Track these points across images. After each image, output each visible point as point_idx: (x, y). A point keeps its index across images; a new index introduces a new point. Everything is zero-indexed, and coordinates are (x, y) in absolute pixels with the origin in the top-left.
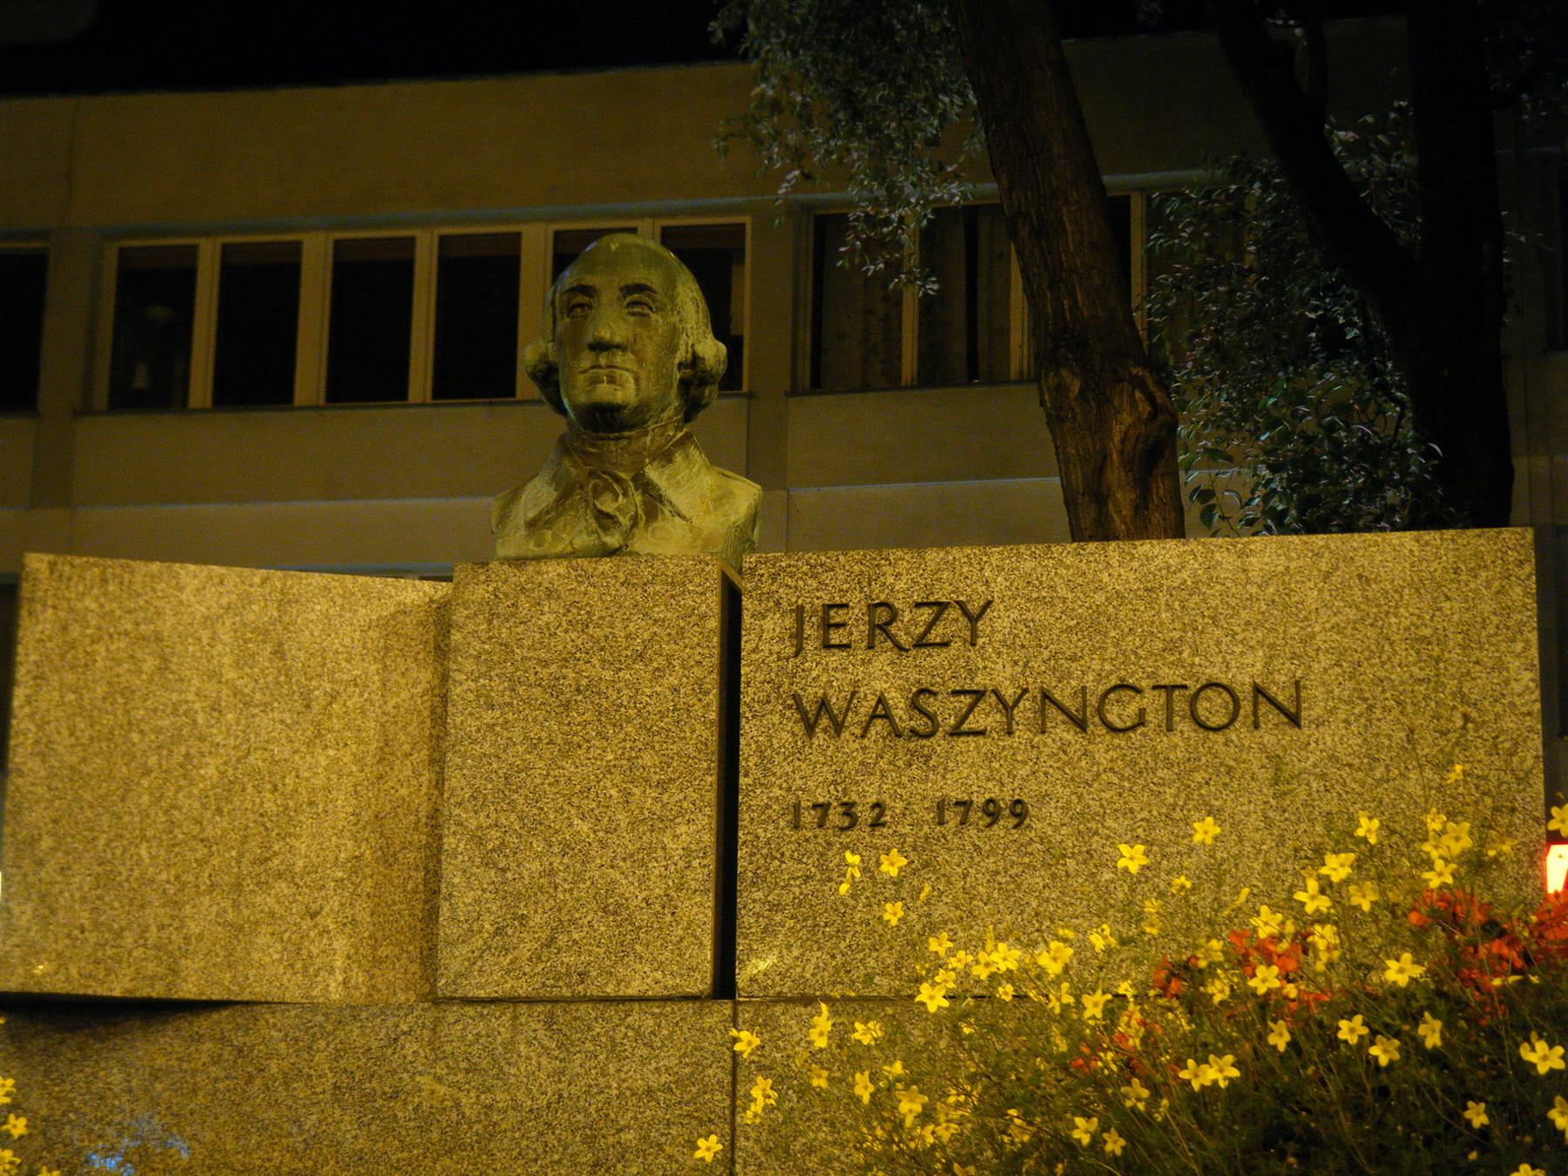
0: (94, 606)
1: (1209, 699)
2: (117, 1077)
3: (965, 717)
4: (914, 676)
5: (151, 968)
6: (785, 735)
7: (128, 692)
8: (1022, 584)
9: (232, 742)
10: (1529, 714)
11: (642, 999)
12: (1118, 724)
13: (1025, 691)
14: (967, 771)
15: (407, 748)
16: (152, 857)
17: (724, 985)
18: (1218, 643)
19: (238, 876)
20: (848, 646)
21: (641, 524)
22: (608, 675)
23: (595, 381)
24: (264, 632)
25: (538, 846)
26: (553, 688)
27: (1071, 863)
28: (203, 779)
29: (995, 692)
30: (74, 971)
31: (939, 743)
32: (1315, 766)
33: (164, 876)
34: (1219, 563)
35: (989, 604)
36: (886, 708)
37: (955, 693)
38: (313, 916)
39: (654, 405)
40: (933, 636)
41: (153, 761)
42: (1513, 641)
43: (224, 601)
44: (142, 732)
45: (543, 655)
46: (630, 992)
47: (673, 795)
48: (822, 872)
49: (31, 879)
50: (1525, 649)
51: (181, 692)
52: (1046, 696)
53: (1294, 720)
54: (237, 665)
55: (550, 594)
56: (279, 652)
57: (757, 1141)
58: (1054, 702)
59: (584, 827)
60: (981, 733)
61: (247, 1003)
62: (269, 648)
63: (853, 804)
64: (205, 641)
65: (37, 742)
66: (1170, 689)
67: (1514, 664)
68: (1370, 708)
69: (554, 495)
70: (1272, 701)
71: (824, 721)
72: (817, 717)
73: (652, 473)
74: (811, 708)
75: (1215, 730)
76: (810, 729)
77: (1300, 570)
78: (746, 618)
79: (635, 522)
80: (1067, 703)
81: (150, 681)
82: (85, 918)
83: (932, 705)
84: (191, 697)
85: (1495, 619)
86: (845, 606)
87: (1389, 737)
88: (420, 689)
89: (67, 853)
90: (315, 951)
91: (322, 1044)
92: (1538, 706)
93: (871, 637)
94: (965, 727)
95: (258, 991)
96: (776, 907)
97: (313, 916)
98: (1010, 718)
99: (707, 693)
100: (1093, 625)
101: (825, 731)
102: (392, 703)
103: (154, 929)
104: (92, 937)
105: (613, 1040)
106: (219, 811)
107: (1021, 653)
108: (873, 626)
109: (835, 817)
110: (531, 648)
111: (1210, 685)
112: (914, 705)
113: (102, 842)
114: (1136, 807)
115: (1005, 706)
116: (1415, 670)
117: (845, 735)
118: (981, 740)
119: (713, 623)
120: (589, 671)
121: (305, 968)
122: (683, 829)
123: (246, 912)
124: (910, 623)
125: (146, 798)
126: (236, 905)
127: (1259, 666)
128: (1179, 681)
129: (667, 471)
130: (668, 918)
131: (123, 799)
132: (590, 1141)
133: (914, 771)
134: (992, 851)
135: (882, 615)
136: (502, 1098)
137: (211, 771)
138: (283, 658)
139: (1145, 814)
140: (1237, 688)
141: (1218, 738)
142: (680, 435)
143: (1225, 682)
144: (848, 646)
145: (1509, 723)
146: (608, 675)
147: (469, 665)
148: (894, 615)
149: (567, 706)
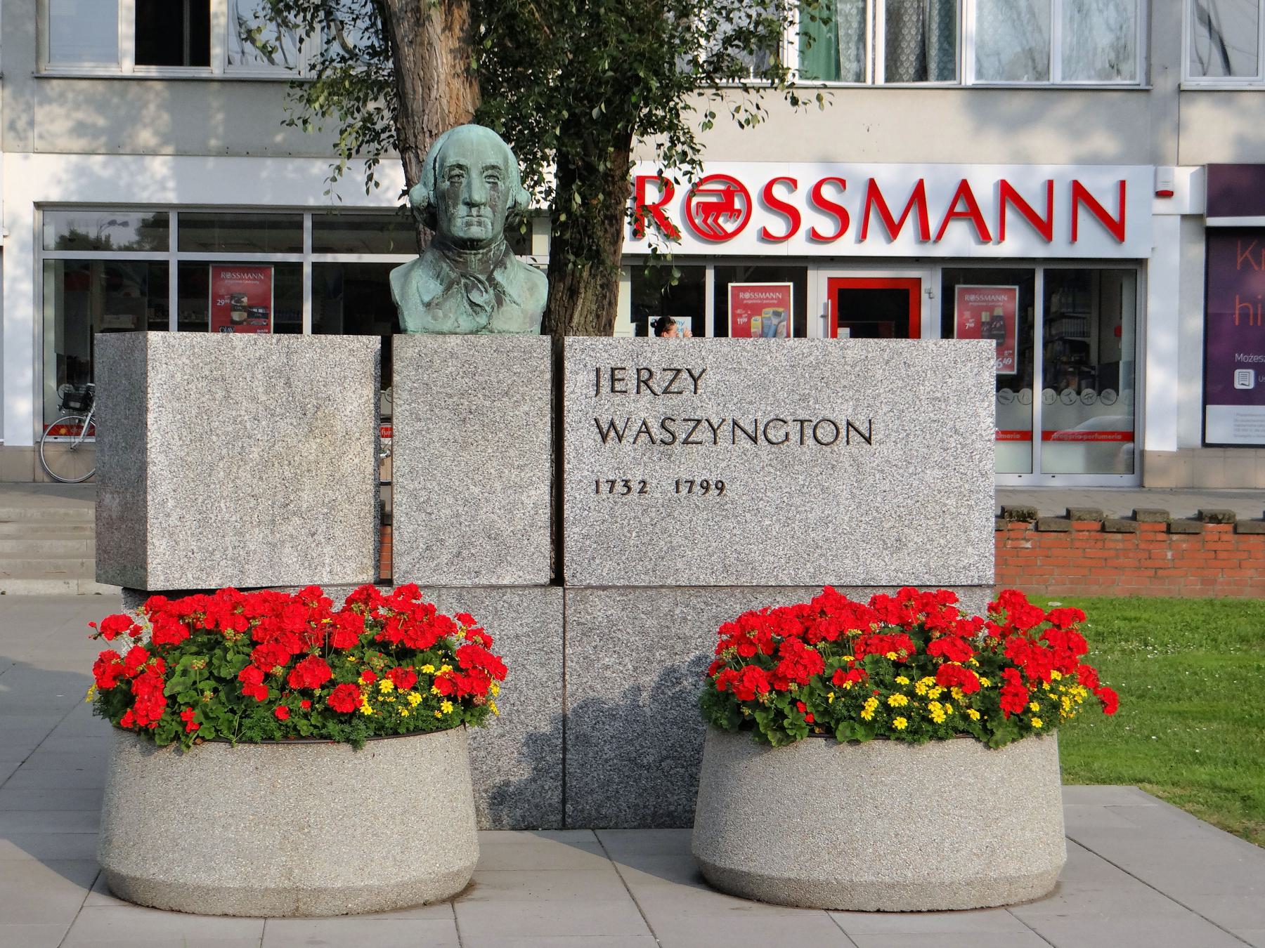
3: (690, 434)
4: (662, 410)
5: (230, 571)
6: (591, 441)
7: (208, 412)
11: (513, 587)
12: (774, 440)
14: (693, 463)
17: (558, 579)
18: (829, 397)
22: (487, 403)
23: (469, 224)
25: (450, 500)
26: (455, 411)
27: (748, 515)
30: (190, 576)
33: (234, 519)
35: (704, 371)
38: (313, 535)
40: (673, 388)
41: (224, 451)
42: (983, 401)
46: (505, 582)
52: (735, 423)
53: (868, 441)
54: (266, 392)
55: (452, 355)
56: (288, 384)
59: (476, 490)
66: (802, 422)
67: (983, 413)
68: (908, 435)
69: (442, 288)
71: (612, 434)
73: (498, 275)
74: (605, 427)
77: (873, 358)
78: (567, 372)
80: (747, 428)
84: (243, 413)
85: (974, 389)
93: (638, 387)
94: (690, 439)
100: (762, 386)
102: (349, 408)
107: (722, 399)
109: (619, 487)
112: (663, 426)
118: (700, 447)
119: (548, 376)
120: (476, 401)
124: (658, 383)
126: (272, 532)
128: (807, 418)
133: (662, 463)
134: (705, 508)
135: (645, 375)
141: (828, 449)
145: (978, 445)
147: (405, 395)
149: (464, 420)
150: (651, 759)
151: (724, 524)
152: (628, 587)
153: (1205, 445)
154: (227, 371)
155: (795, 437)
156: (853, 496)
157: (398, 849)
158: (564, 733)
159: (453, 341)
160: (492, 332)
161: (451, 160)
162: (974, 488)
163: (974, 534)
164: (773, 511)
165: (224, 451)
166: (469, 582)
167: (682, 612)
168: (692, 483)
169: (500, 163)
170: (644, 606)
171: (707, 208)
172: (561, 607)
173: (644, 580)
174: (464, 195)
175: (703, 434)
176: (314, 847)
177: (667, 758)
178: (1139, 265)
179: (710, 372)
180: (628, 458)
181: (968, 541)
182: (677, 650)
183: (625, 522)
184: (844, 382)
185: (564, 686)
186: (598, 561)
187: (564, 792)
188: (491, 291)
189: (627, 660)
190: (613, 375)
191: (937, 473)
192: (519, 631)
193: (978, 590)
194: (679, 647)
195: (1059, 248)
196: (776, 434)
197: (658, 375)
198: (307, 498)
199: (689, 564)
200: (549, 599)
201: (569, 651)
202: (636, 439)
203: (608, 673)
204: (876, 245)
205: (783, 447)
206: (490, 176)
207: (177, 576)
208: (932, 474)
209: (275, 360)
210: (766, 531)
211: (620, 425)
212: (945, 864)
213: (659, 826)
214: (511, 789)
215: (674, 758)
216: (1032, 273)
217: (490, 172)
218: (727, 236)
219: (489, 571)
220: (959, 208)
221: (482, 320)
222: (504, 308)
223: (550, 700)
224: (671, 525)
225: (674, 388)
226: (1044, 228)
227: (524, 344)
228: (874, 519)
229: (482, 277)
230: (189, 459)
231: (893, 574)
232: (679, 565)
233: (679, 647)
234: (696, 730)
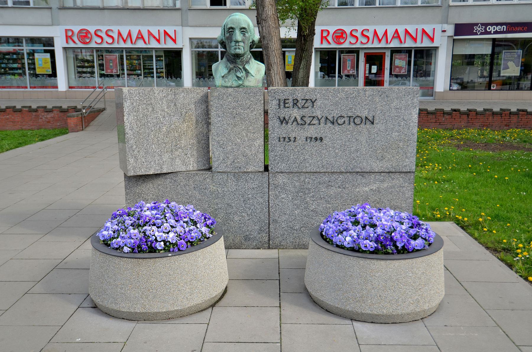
2: (151, 185)
4: (302, 113)
11: (251, 172)
12: (340, 123)
14: (312, 131)
17: (266, 168)
22: (242, 111)
25: (230, 144)
27: (331, 149)
41: (153, 129)
53: (373, 123)
55: (230, 95)
56: (175, 105)
66: (350, 117)
71: (285, 121)
72: (283, 121)
73: (247, 67)
74: (282, 119)
76: (282, 123)
82: (144, 160)
83: (305, 119)
95: (178, 170)
96: (276, 156)
104: (146, 164)
109: (287, 140)
126: (172, 154)
133: (302, 131)
135: (295, 102)
136: (226, 189)
141: (359, 126)
145: (412, 124)
146: (242, 111)
147: (214, 109)
150: (297, 227)
151: (323, 151)
152: (290, 172)
153: (450, 90)
155: (347, 122)
157: (189, 294)
159: (230, 90)
161: (229, 26)
163: (409, 155)
165: (153, 129)
169: (246, 26)
170: (296, 179)
171: (337, 37)
174: (234, 39)
175: (315, 121)
176: (154, 297)
178: (436, 48)
182: (306, 193)
184: (365, 103)
187: (269, 237)
188: (244, 72)
191: (396, 134)
193: (409, 174)
194: (307, 192)
195: (419, 45)
196: (340, 121)
199: (310, 165)
200: (264, 176)
204: (376, 45)
206: (243, 31)
211: (287, 118)
212: (399, 307)
213: (300, 248)
216: (411, 51)
217: (243, 30)
218: (342, 43)
220: (395, 35)
221: (241, 82)
222: (249, 78)
226: (415, 40)
229: (241, 67)
232: (307, 165)
233: (307, 192)
234: (312, 218)
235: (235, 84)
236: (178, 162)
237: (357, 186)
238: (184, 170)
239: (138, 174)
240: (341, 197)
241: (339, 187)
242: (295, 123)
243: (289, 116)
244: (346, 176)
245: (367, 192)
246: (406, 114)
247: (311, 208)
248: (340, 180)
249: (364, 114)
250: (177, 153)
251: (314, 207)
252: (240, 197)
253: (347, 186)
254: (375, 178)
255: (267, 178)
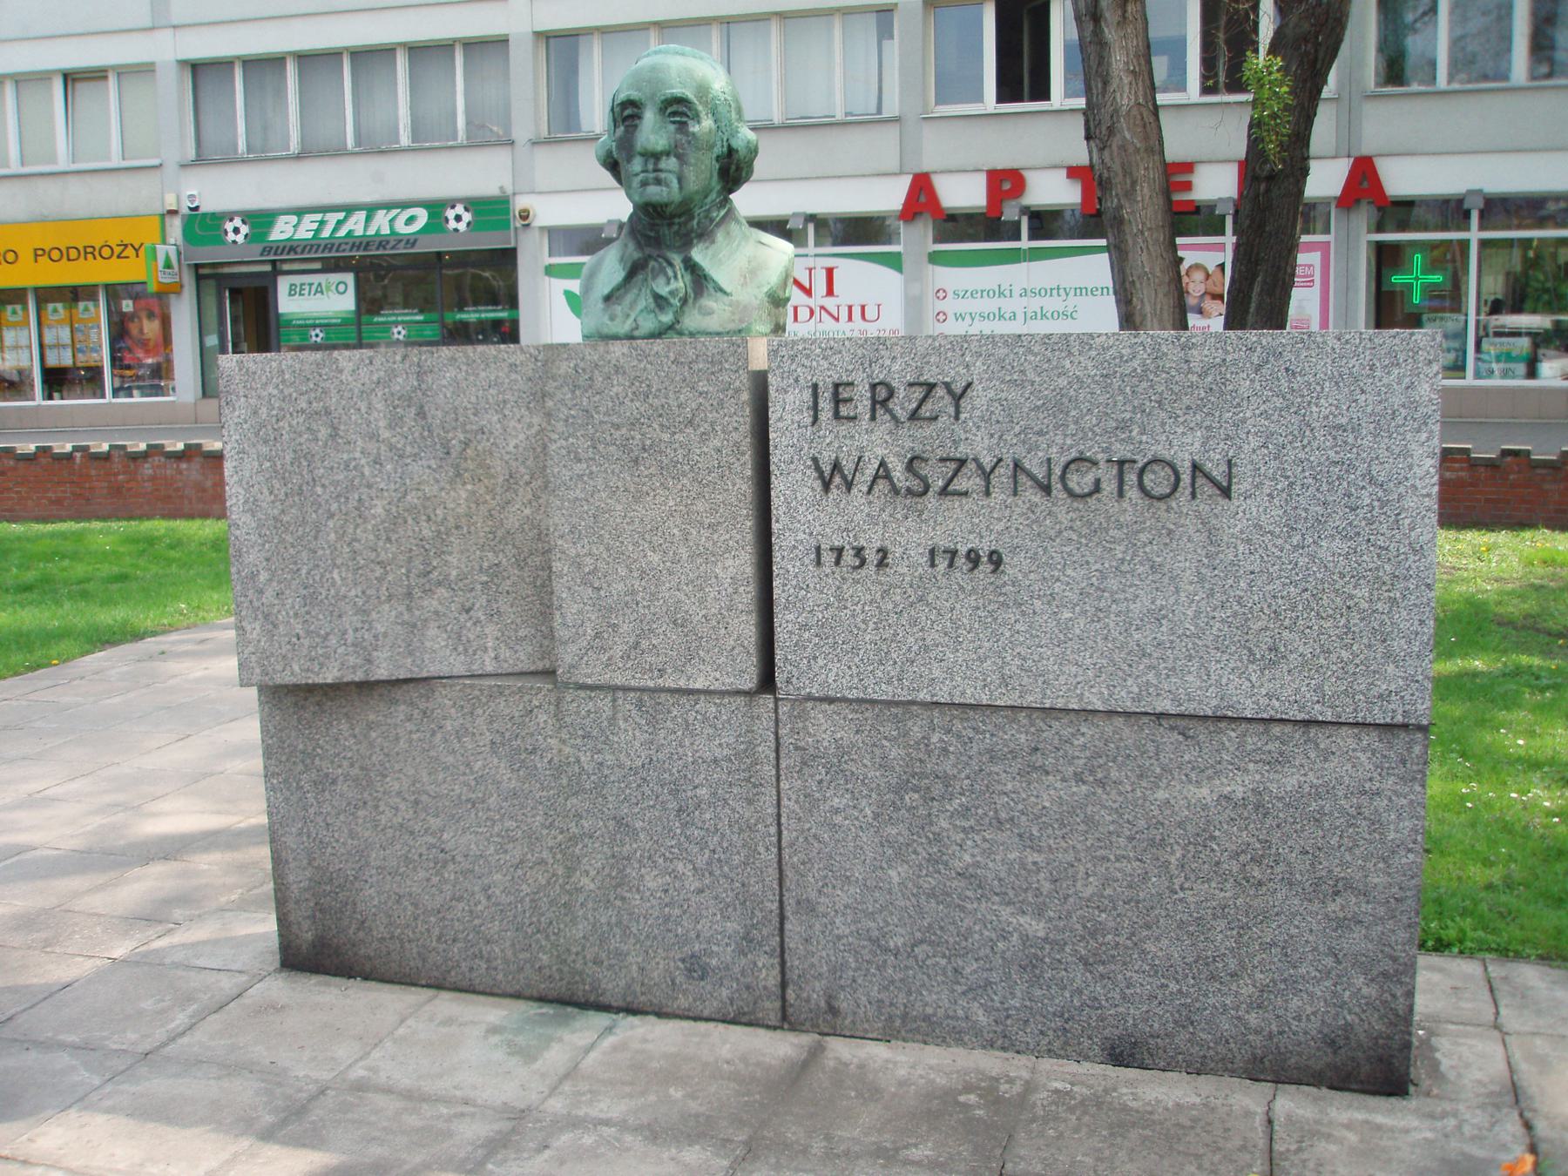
0: (275, 392)
1: (1154, 472)
2: (344, 726)
3: (951, 480)
5: (352, 660)
6: (807, 491)
7: (310, 457)
8: (997, 368)
9: (392, 486)
10: (1428, 495)
11: (707, 692)
12: (1077, 490)
13: (1000, 460)
14: (957, 524)
15: (527, 477)
16: (343, 579)
17: (767, 682)
18: (1163, 424)
19: (409, 586)
20: (855, 418)
21: (691, 301)
22: (666, 437)
24: (408, 400)
25: (622, 572)
26: (625, 447)
28: (374, 517)
29: (975, 460)
30: (296, 668)
31: (931, 500)
32: (1242, 532)
33: (353, 593)
34: (1165, 354)
35: (969, 385)
36: (887, 471)
37: (943, 460)
38: (468, 611)
39: (697, 198)
41: (334, 507)
42: (1419, 431)
43: (375, 378)
44: (323, 486)
45: (615, 419)
46: (698, 686)
47: (722, 535)
48: (840, 601)
49: (256, 604)
50: (1428, 439)
51: (349, 452)
52: (1017, 466)
53: (1226, 492)
54: (390, 427)
56: (421, 414)
57: (797, 802)
58: (1024, 470)
59: (655, 558)
60: (966, 494)
61: (425, 679)
62: (413, 410)
63: (863, 548)
64: (363, 410)
65: (246, 502)
66: (1121, 463)
67: (1418, 452)
70: (1208, 476)
71: (837, 480)
72: (831, 477)
73: (698, 254)
74: (827, 469)
75: (1160, 498)
76: (826, 486)
77: (1235, 363)
79: (684, 301)
80: (1035, 471)
81: (325, 445)
82: (299, 629)
83: (925, 470)
84: (358, 455)
86: (851, 384)
87: (1306, 510)
88: (533, 431)
89: (280, 582)
90: (472, 637)
91: (480, 711)
92: (1436, 489)
93: (873, 410)
94: (951, 488)
95: (432, 669)
96: (805, 627)
97: (468, 611)
98: (988, 482)
99: (743, 454)
100: (1058, 406)
101: (838, 487)
102: (512, 443)
103: (350, 631)
104: (306, 642)
105: (686, 721)
106: (389, 540)
108: (874, 402)
109: (849, 558)
110: (606, 414)
111: (1155, 461)
112: (910, 467)
113: (304, 571)
114: (1091, 560)
115: (984, 472)
116: (1331, 454)
117: (854, 491)
121: (466, 650)
122: (730, 562)
123: (417, 613)
124: (903, 403)
125: (333, 536)
126: (409, 609)
127: (1197, 445)
128: (1129, 456)
129: (710, 252)
130: (723, 631)
131: (316, 538)
132: (675, 793)
133: (909, 523)
135: (882, 393)
136: (610, 759)
137: (379, 510)
138: (424, 418)
139: (1098, 566)
140: (1178, 463)
141: (1162, 506)
142: (722, 213)
143: (1168, 458)
144: (855, 418)
146: (666, 437)
148: (891, 393)
149: (636, 461)
150: (900, 941)
154: (333, 401)
155: (1109, 487)
156: (1202, 580)
158: (781, 895)
160: (681, 334)
162: (1400, 572)
163: (1398, 645)
164: (1075, 598)
165: (334, 507)
166: (651, 684)
167: (941, 740)
168: (954, 553)
170: (889, 729)
172: (772, 724)
173: (885, 692)
175: (968, 481)
177: (922, 942)
179: (978, 388)
180: (860, 516)
181: (1388, 655)
183: (858, 608)
184: (1186, 400)
185: (780, 833)
186: (821, 662)
187: (783, 973)
189: (864, 802)
190: (836, 394)
192: (718, 753)
194: (938, 789)
196: (1081, 481)
197: (901, 393)
198: (455, 563)
200: (756, 711)
201: (784, 785)
202: (870, 489)
203: (838, 819)
205: (1092, 501)
207: (279, 668)
208: (1330, 548)
209: (400, 384)
210: (1066, 628)
211: (848, 466)
214: (1248, 53)
215: (931, 943)
219: (676, 669)
221: (667, 318)
223: (761, 849)
224: (922, 613)
225: (926, 411)
227: (712, 350)
228: (1235, 615)
230: (285, 519)
231: (1264, 701)
232: (936, 673)
233: (938, 789)
234: (962, 909)
235: (648, 324)
236: (435, 638)
237: (1159, 777)
238: (459, 669)
239: (279, 681)
240: (1089, 821)
241: (1079, 778)
242: (882, 485)
243: (856, 454)
244: (1109, 730)
245: (1205, 807)
246: (1383, 454)
247: (958, 865)
248: (1084, 746)
249: (1185, 448)
250: (431, 603)
251: (967, 858)
252: (666, 796)
253: (1114, 774)
254: (1241, 745)
255: (766, 722)
